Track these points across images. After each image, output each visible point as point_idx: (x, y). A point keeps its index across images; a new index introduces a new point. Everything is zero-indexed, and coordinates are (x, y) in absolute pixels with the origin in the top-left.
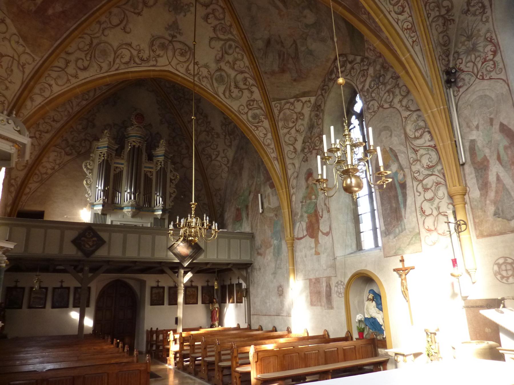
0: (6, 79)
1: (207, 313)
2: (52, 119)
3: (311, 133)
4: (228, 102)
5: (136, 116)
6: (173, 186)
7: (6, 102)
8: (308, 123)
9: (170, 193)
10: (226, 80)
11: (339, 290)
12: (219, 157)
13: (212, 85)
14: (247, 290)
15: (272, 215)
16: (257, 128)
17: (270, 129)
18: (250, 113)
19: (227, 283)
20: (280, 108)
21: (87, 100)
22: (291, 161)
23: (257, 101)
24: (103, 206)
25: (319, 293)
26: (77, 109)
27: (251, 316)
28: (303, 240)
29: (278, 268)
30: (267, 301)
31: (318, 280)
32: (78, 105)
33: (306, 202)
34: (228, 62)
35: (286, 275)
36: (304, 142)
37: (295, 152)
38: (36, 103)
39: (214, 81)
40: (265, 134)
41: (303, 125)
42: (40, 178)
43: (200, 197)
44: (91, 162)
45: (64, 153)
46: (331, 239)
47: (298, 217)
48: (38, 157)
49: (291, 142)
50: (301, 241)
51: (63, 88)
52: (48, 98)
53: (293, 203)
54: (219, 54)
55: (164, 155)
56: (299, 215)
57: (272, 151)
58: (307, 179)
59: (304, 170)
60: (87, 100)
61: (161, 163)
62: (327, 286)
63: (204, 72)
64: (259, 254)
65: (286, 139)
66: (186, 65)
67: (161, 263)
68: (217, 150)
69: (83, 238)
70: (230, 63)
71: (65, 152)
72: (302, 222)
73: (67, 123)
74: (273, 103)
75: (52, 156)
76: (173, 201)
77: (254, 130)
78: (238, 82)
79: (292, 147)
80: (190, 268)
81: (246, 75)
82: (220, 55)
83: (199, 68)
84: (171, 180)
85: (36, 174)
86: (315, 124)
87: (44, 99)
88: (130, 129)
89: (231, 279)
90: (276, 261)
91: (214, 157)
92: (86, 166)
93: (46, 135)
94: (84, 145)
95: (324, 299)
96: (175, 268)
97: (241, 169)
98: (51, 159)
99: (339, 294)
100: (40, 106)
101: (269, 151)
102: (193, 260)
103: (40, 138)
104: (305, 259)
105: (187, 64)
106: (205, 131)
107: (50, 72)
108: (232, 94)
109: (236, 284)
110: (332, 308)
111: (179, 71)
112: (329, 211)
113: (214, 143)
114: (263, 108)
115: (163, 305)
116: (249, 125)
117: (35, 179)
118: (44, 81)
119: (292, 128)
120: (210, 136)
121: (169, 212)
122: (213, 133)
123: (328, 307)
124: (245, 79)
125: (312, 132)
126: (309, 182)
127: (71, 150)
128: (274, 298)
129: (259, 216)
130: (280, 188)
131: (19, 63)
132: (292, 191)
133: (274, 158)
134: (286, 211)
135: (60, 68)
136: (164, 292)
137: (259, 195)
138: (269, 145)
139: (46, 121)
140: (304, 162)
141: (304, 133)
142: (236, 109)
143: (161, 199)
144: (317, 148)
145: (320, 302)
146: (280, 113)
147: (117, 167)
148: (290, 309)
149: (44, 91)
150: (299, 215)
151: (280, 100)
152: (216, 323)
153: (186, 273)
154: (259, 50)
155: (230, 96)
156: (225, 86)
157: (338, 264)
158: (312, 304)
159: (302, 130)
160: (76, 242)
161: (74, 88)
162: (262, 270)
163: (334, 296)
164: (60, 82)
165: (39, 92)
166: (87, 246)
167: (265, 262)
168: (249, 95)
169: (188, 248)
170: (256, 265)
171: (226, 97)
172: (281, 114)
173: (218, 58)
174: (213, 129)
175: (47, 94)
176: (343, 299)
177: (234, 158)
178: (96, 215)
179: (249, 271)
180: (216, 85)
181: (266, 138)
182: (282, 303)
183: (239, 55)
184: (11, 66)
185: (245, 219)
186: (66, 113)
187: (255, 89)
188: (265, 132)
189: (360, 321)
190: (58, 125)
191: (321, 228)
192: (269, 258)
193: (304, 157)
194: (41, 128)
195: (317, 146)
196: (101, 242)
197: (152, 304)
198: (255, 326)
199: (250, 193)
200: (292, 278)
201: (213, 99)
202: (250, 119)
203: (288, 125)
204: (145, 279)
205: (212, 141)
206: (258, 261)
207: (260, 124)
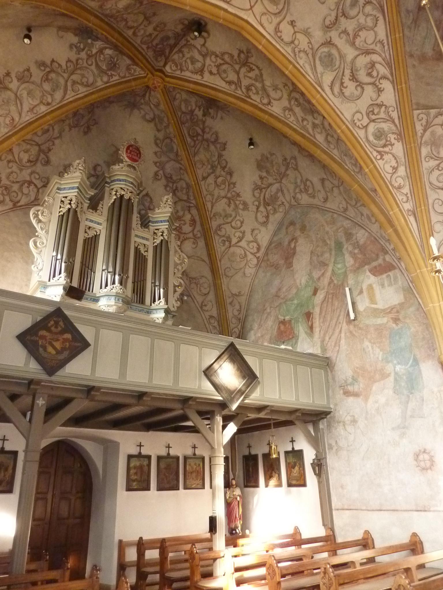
4: (336, 101)
5: (128, 148)
9: (175, 286)
10: (338, 63)
12: (243, 241)
13: (314, 68)
16: (382, 156)
17: (403, 160)
18: (372, 128)
20: (427, 122)
21: (48, 104)
23: (386, 107)
26: (28, 118)
27: (334, 513)
32: (31, 110)
34: (345, 32)
39: (318, 62)
40: (394, 168)
43: (205, 305)
54: (330, 15)
57: (405, 199)
60: (48, 104)
61: (163, 232)
63: (303, 41)
66: (276, 20)
68: (242, 229)
69: (43, 333)
70: (348, 34)
74: (416, 112)
77: (376, 158)
78: (357, 70)
81: (375, 58)
82: (333, 18)
83: (295, 32)
84: (176, 265)
88: (116, 167)
91: (234, 240)
92: (36, 216)
94: (25, 190)
101: (400, 198)
105: (278, 20)
106: (225, 197)
108: (344, 90)
111: (264, 28)
113: (238, 218)
114: (397, 121)
115: (149, 490)
116: (369, 149)
120: (232, 206)
122: (237, 202)
124: (373, 65)
133: (409, 210)
136: (149, 465)
137: (347, 289)
142: (349, 117)
146: (425, 131)
151: (427, 107)
154: (408, 11)
155: (342, 93)
156: (335, 73)
160: (28, 339)
162: (361, 424)
166: (50, 349)
168: (374, 96)
171: (333, 94)
172: (428, 133)
173: (327, 23)
174: (238, 195)
179: (321, 426)
180: (320, 69)
181: (395, 176)
183: (369, 19)
187: (386, 85)
196: (79, 344)
197: (129, 489)
201: (314, 92)
202: (371, 138)
203: (438, 153)
206: (346, 408)
207: (386, 149)
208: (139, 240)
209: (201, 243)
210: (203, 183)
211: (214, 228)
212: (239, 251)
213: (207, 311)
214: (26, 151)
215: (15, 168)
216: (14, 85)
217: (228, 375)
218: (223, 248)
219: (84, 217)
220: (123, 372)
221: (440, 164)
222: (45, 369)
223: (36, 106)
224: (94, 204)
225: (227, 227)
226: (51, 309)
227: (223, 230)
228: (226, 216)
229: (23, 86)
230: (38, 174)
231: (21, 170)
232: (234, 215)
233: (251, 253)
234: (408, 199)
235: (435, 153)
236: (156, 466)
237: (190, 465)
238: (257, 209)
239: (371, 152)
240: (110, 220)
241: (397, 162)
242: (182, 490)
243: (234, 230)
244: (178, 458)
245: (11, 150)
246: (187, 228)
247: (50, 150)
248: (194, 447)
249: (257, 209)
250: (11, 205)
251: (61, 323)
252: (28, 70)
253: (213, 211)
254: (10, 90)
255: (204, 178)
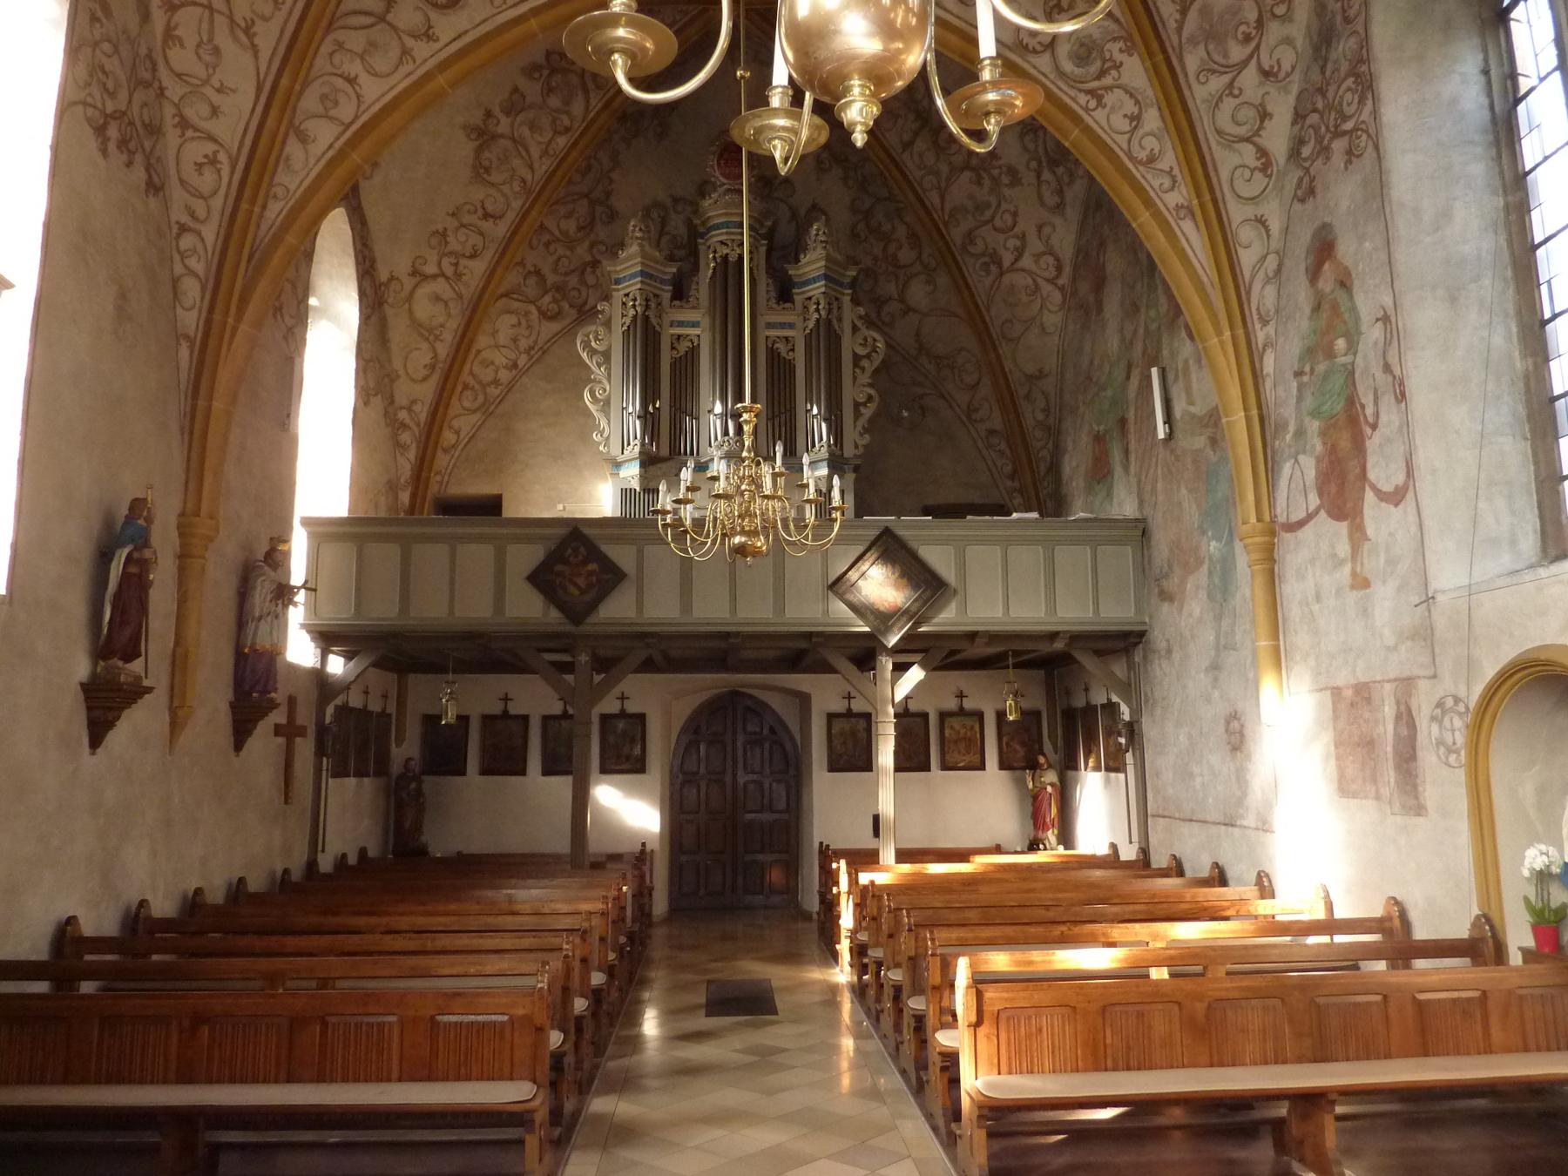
0: (206, 82)
1: (1021, 801)
2: (480, 212)
3: (1323, 70)
6: (865, 379)
7: (222, 157)
8: (1308, 27)
9: (857, 405)
11: (1449, 739)
12: (1026, 254)
14: (1133, 730)
15: (1200, 441)
16: (1099, 98)
17: (1150, 92)
19: (1079, 702)
21: (567, 130)
22: (1250, 211)
24: (643, 465)
25: (1368, 744)
26: (544, 168)
28: (1307, 532)
29: (1224, 646)
30: (1196, 770)
31: (1363, 694)
32: (545, 153)
33: (1312, 370)
35: (1251, 675)
36: (1299, 116)
37: (1265, 168)
38: (318, 148)
41: (1288, 41)
42: (481, 399)
43: (976, 410)
44: (601, 330)
45: (535, 311)
46: (1412, 518)
47: (1288, 437)
48: (463, 336)
49: (1242, 131)
50: (1301, 534)
51: (392, 81)
52: (352, 122)
53: (1269, 384)
55: (826, 277)
56: (1292, 428)
57: (1167, 183)
58: (1314, 274)
59: (1304, 237)
60: (567, 130)
62: (1398, 717)
64: (1166, 596)
65: (1224, 119)
67: (810, 635)
69: (559, 568)
71: (539, 309)
72: (1301, 458)
73: (524, 215)
75: (505, 326)
76: (866, 430)
79: (1248, 151)
80: (916, 648)
84: (857, 359)
85: (466, 387)
86: (1339, 18)
87: (341, 128)
88: (706, 203)
89: (1087, 690)
90: (1219, 618)
91: (1007, 259)
92: (587, 345)
93: (471, 263)
95: (1390, 774)
96: (864, 653)
97: (1099, 285)
98: (502, 338)
99: (1450, 751)
100: (331, 153)
101: (1156, 184)
102: (917, 624)
103: (458, 275)
104: (1315, 607)
107: (340, 35)
109: (1103, 706)
110: (1419, 810)
112: (1402, 397)
113: (1004, 206)
117: (467, 404)
118: (329, 69)
119: (1245, 63)
120: (987, 182)
121: (856, 469)
122: (996, 172)
123: (1403, 806)
125: (1326, 60)
126: (1320, 285)
127: (555, 301)
128: (1216, 759)
129: (1162, 453)
130: (1208, 327)
131: (232, 21)
132: (1261, 335)
133: (1178, 207)
134: (1237, 422)
135: (366, 13)
137: (1154, 371)
138: (1151, 159)
139: (465, 221)
140: (1302, 201)
141: (1296, 76)
143: (824, 426)
144: (1348, 126)
145: (1375, 781)
147: (679, 336)
148: (1268, 805)
149: (336, 103)
150: (1292, 428)
152: (1051, 836)
153: (901, 668)
157: (1440, 622)
158: (1345, 788)
159: (1286, 66)
160: (541, 579)
161: (428, 76)
162: (1176, 656)
163: (1428, 759)
164: (381, 63)
165: (321, 110)
166: (573, 590)
167: (1186, 623)
169: (897, 587)
170: (1158, 638)
172: (1193, 15)
175: (346, 111)
176: (1461, 776)
177: (1079, 250)
178: (626, 494)
181: (1140, 132)
182: (1241, 779)
184: (211, 40)
185: (1118, 470)
186: (516, 187)
188: (1130, 107)
189: (1543, 877)
190: (500, 230)
191: (1372, 475)
192: (1197, 612)
193: (1301, 180)
194: (454, 245)
195: (1345, 118)
196: (612, 576)
197: (834, 767)
198: (1159, 860)
199: (1129, 367)
200: (1268, 684)
202: (1068, 66)
203: (1226, 56)
204: (804, 688)
205: (993, 200)
208: (773, 333)
209: (943, 280)
210: (906, 156)
211: (959, 242)
212: (1021, 280)
213: (982, 420)
214: (569, 215)
215: (561, 251)
216: (504, 125)
217: (878, 585)
218: (988, 281)
219: (666, 319)
220: (686, 606)
221: (1233, 80)
222: (568, 617)
223: (550, 142)
224: (680, 293)
225: (985, 231)
226: (563, 531)
227: (979, 242)
228: (977, 208)
229: (519, 119)
230: (601, 242)
231: (572, 249)
232: (994, 204)
233: (1047, 280)
234: (1174, 181)
235: (1217, 57)
236: (825, 737)
237: (952, 728)
238: (1039, 177)
239: (1073, 99)
240: (712, 312)
241: (1137, 102)
242: (936, 771)
243: (1002, 237)
244: (925, 716)
245: (542, 226)
246: (906, 255)
247: (608, 194)
248: (961, 696)
249: (1039, 177)
250: (573, 312)
251: (582, 550)
252: (516, 90)
253: (948, 206)
254: (502, 136)
255: (907, 146)
